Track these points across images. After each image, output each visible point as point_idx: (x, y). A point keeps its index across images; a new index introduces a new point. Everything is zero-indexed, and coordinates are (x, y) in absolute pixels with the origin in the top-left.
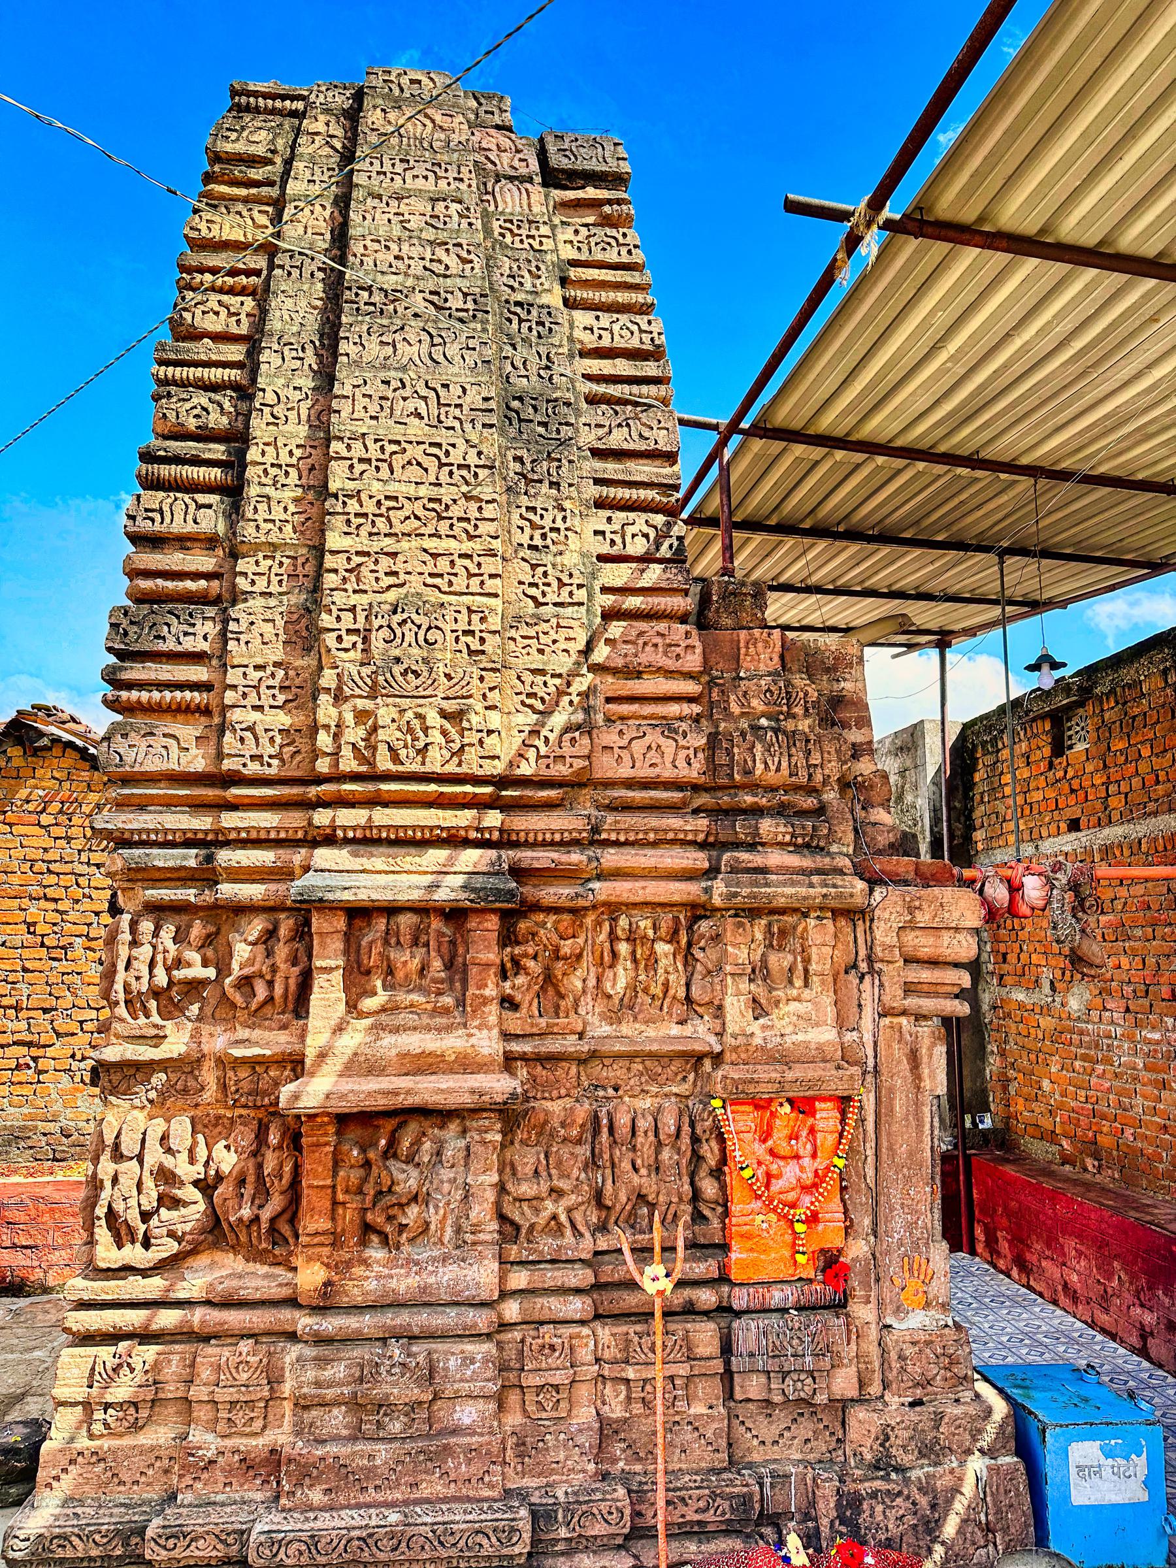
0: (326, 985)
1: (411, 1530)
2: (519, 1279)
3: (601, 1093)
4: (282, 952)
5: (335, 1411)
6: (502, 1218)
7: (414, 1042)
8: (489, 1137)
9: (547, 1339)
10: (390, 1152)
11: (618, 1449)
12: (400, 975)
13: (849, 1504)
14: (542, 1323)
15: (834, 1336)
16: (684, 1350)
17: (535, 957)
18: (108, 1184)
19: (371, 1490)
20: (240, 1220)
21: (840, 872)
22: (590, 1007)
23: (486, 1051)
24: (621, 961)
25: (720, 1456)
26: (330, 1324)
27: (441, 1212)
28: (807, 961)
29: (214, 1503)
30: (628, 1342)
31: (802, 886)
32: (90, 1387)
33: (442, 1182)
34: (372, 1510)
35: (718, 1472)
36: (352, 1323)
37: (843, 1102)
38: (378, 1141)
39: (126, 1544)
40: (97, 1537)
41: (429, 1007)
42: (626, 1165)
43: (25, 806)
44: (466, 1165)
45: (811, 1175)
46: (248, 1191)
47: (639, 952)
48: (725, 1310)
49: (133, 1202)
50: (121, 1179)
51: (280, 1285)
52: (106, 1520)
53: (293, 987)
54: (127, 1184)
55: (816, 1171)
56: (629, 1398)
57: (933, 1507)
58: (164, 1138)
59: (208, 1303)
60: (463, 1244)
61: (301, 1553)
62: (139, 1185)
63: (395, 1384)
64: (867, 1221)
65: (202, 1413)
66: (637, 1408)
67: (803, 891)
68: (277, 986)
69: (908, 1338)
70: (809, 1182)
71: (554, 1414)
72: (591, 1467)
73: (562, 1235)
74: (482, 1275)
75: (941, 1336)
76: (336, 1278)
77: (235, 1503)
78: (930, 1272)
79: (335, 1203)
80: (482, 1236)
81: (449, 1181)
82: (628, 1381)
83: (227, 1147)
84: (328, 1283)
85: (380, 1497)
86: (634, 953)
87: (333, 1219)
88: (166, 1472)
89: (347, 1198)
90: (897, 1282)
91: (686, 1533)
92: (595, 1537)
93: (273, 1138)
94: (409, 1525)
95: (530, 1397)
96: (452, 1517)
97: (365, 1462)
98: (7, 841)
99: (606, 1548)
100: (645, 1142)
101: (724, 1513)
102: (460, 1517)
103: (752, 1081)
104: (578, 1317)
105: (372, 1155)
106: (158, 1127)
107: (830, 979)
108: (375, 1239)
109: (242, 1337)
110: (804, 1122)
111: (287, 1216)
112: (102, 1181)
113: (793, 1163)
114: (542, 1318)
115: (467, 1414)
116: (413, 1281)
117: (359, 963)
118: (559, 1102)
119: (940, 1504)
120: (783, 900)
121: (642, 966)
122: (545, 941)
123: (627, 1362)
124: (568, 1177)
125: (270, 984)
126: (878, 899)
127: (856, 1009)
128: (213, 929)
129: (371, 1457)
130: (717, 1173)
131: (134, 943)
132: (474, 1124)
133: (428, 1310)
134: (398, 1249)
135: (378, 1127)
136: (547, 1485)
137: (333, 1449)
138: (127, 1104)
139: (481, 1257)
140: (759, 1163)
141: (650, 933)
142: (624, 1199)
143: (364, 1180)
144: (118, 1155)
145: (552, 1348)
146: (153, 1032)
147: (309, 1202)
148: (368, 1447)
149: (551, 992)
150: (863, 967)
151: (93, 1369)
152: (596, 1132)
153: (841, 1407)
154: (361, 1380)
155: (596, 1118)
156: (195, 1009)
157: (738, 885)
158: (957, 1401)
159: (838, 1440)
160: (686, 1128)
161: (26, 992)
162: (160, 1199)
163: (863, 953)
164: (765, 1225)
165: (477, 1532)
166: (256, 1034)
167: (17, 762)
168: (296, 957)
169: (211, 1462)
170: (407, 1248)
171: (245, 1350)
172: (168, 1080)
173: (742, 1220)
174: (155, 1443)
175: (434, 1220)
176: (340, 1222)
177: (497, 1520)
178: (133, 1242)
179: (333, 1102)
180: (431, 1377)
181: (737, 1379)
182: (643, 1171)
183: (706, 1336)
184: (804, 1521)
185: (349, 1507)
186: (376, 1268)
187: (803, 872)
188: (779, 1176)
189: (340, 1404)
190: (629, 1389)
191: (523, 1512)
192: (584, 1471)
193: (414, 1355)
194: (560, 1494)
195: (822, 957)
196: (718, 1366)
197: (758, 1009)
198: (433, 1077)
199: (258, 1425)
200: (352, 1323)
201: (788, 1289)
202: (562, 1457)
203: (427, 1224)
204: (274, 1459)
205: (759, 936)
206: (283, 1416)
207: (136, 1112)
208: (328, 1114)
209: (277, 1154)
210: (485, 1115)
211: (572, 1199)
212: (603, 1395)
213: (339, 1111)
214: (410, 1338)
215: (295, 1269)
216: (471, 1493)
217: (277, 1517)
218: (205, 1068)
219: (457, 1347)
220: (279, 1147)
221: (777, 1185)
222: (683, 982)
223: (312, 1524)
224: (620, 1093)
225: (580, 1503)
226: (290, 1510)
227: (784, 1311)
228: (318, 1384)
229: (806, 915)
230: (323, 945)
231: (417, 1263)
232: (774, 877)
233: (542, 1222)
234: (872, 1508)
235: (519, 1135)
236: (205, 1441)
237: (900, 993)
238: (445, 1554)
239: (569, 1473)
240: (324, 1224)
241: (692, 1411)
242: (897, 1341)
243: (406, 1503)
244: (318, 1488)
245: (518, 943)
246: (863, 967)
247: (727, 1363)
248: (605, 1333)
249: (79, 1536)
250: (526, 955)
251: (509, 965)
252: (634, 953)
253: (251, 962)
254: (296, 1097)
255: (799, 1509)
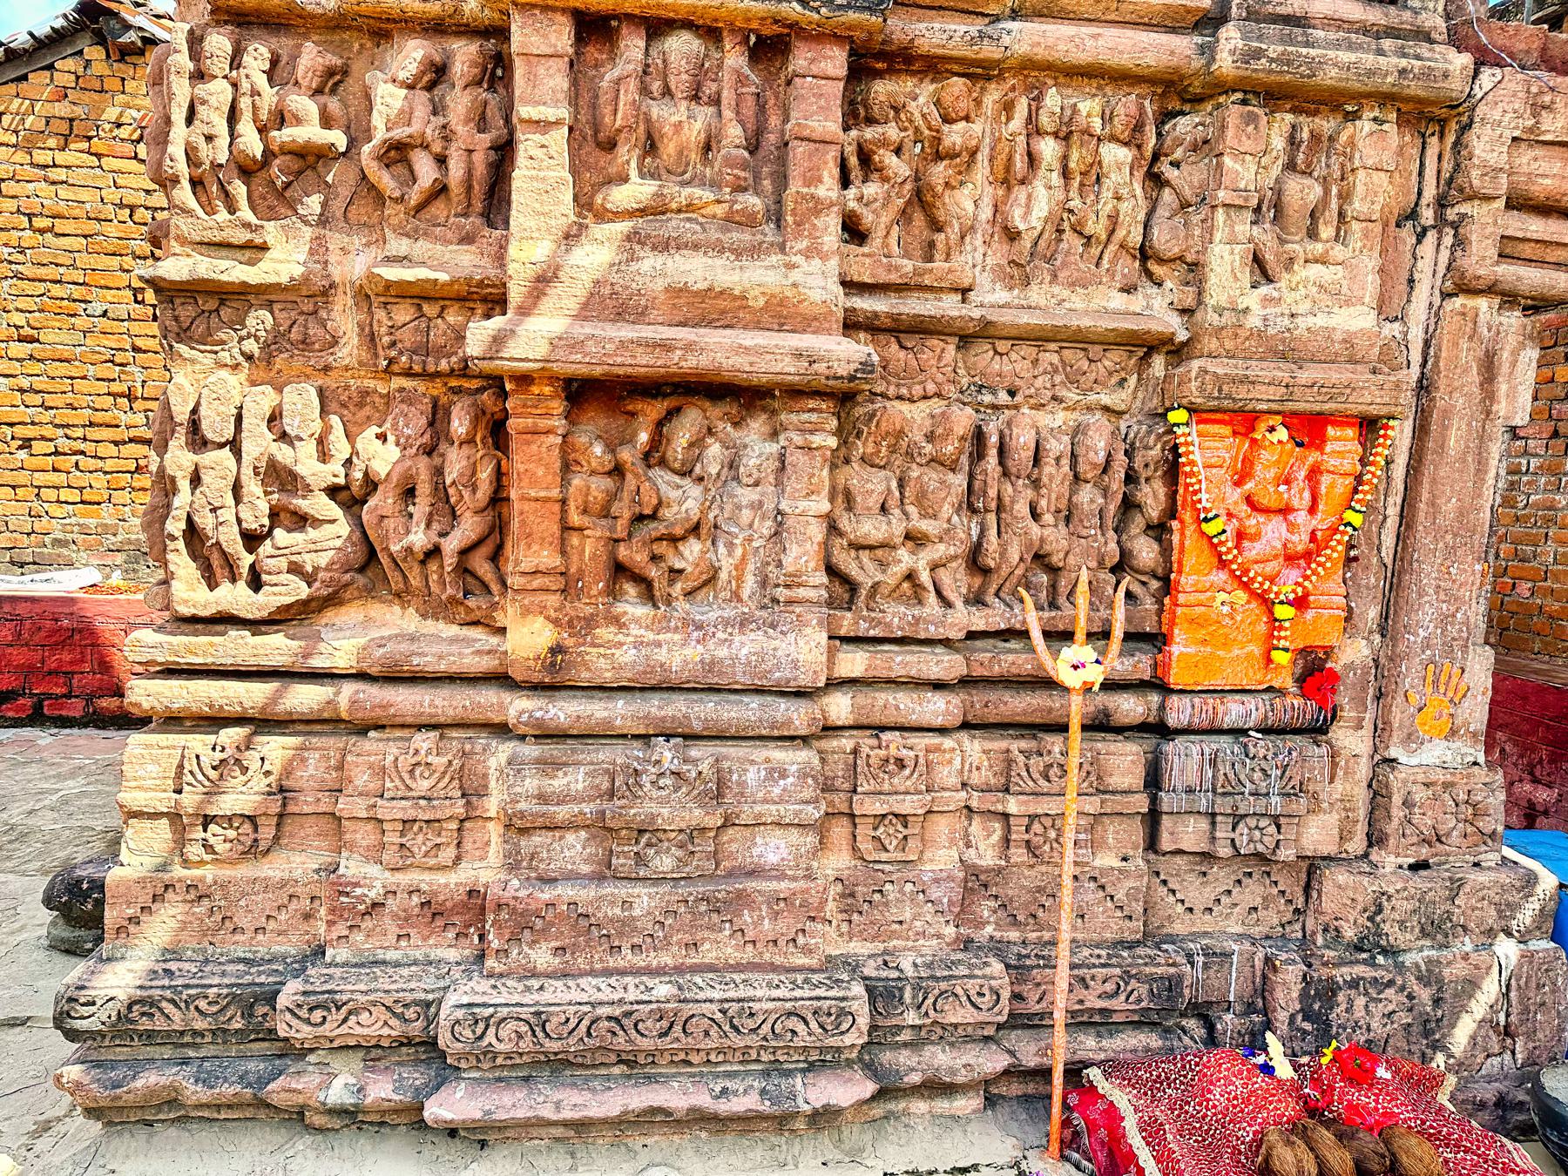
0: (539, 153)
1: (689, 1009)
2: (854, 662)
3: (987, 398)
4: (460, 102)
5: (570, 837)
6: (832, 570)
7: (696, 270)
8: (817, 440)
9: (893, 751)
10: (654, 455)
11: (985, 908)
12: (669, 149)
13: (1319, 998)
14: (883, 729)
15: (1312, 770)
16: (1093, 778)
17: (898, 151)
18: (184, 485)
19: (626, 951)
20: (409, 550)
21: (1425, 36)
22: (979, 258)
23: (816, 296)
24: (1042, 172)
25: (1134, 924)
26: (563, 711)
27: (739, 552)
28: (1345, 197)
29: (384, 962)
30: (1009, 762)
31: (1368, 51)
32: (179, 792)
33: (739, 507)
34: (628, 979)
35: (1131, 946)
36: (597, 710)
37: (1369, 426)
38: (634, 435)
39: (248, 1012)
40: (202, 1004)
41: (720, 210)
42: (1022, 508)
43: (116, 132)
44: (779, 483)
45: (1306, 537)
46: (420, 508)
47: (1074, 155)
48: (1158, 729)
49: (228, 515)
50: (206, 478)
51: (478, 652)
52: (216, 981)
53: (480, 169)
54: (216, 484)
55: (1313, 533)
56: (1007, 841)
57: (1437, 1002)
58: (274, 418)
59: (362, 676)
60: (775, 602)
61: (520, 1036)
62: (237, 489)
63: (662, 802)
64: (1373, 613)
65: (363, 835)
66: (1019, 854)
67: (1369, 60)
68: (452, 163)
69: (1421, 778)
70: (1300, 548)
71: (900, 856)
72: (950, 931)
73: (920, 602)
74: (803, 649)
75: (1468, 776)
76: (570, 642)
77: (415, 963)
78: (1463, 687)
79: (566, 528)
80: (802, 593)
81: (752, 506)
82: (1006, 816)
83: (382, 437)
84: (557, 650)
85: (639, 961)
86: (1065, 158)
87: (563, 553)
88: (307, 916)
89: (585, 521)
90: (1415, 699)
91: (1082, 1023)
92: (956, 1026)
93: (459, 425)
94: (685, 1001)
95: (864, 830)
96: (750, 993)
97: (618, 911)
98: (95, 177)
99: (969, 1039)
100: (1055, 475)
101: (1139, 1000)
102: (763, 992)
103: (1245, 380)
104: (939, 722)
105: (626, 455)
106: (262, 400)
107: (1378, 228)
108: (631, 589)
109: (419, 727)
110: (1303, 459)
111: (485, 550)
112: (173, 480)
113: (1277, 520)
114: (885, 721)
115: (773, 849)
116: (694, 652)
117: (596, 127)
118: (922, 405)
119: (1448, 998)
120: (1334, 72)
121: (1076, 184)
122: (919, 121)
123: (1007, 790)
124: (935, 517)
125: (441, 160)
126: (1487, 86)
127: (1404, 287)
128: (334, 60)
129: (627, 904)
130: (1159, 530)
131: (199, 76)
132: (794, 417)
133: (716, 697)
134: (669, 604)
135: (633, 414)
136: (886, 952)
137: (566, 892)
138: (208, 360)
139: (801, 623)
140: (1230, 515)
141: (1097, 123)
142: (1014, 556)
143: (613, 497)
144: (198, 441)
145: (901, 763)
146: (242, 236)
147: (523, 523)
148: (623, 890)
149: (919, 219)
150: (1428, 216)
151: (181, 766)
152: (979, 454)
153: (1312, 868)
154: (611, 794)
155: (979, 436)
156: (313, 203)
157: (1260, 38)
158: (1476, 865)
159: (1297, 911)
160: (1120, 460)
161: (139, 378)
162: (274, 515)
163: (1430, 192)
164: (1226, 609)
165: (789, 1014)
166: (422, 248)
167: (99, 68)
168: (483, 117)
169: (374, 905)
170: (682, 605)
171: (425, 746)
172: (276, 324)
173: (1192, 598)
174: (286, 875)
175: (727, 565)
176: (575, 558)
177: (818, 998)
178: (234, 580)
179: (560, 354)
180: (719, 795)
181: (1166, 822)
182: (1048, 518)
183: (1125, 761)
184: (1246, 1014)
185: (592, 973)
186: (635, 630)
187: (1365, 30)
188: (1256, 537)
189: (577, 828)
190: (1008, 829)
191: (858, 989)
192: (939, 936)
193: (695, 762)
194: (907, 965)
195: (1374, 192)
196: (1141, 803)
197: (1261, 269)
198: (728, 332)
199: (448, 854)
200: (597, 710)
201: (1251, 702)
202: (907, 916)
203: (717, 570)
204: (475, 905)
205: (1279, 143)
206: (488, 843)
207: (224, 373)
208: (552, 379)
209: (466, 450)
210: (812, 404)
211: (939, 551)
212: (967, 835)
213: (570, 369)
214: (686, 737)
215: (502, 631)
216: (778, 960)
217: (485, 985)
218: (338, 308)
219: (760, 753)
220: (469, 441)
221: (1253, 550)
222: (1141, 217)
223: (536, 997)
224: (1019, 398)
225: (937, 979)
226: (501, 975)
227: (1238, 732)
228: (542, 798)
229: (1353, 117)
230: (532, 78)
231: (699, 627)
232: (1320, 34)
233: (892, 582)
234: (1350, 1001)
235: (860, 448)
236: (366, 874)
237: (1493, 253)
238: (739, 1042)
239: (919, 940)
240: (548, 558)
241: (1097, 863)
242: (1405, 782)
243: (679, 970)
244: (544, 945)
245: (871, 121)
246: (1428, 216)
247: (1154, 800)
248: (974, 747)
249: (172, 1001)
250: (884, 143)
251: (853, 161)
252: (1065, 158)
253: (406, 116)
254: (499, 340)
255: (1240, 998)
